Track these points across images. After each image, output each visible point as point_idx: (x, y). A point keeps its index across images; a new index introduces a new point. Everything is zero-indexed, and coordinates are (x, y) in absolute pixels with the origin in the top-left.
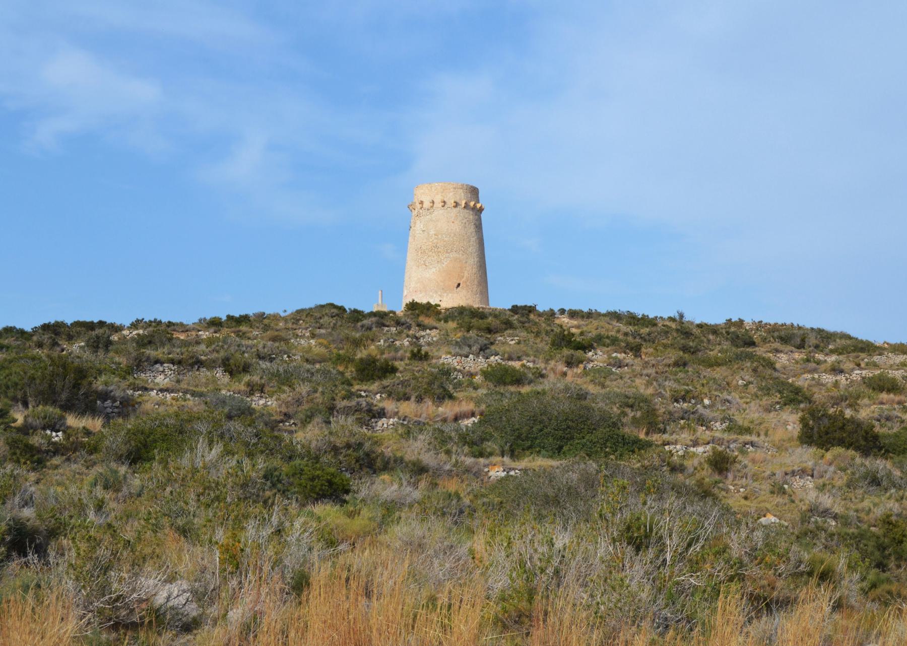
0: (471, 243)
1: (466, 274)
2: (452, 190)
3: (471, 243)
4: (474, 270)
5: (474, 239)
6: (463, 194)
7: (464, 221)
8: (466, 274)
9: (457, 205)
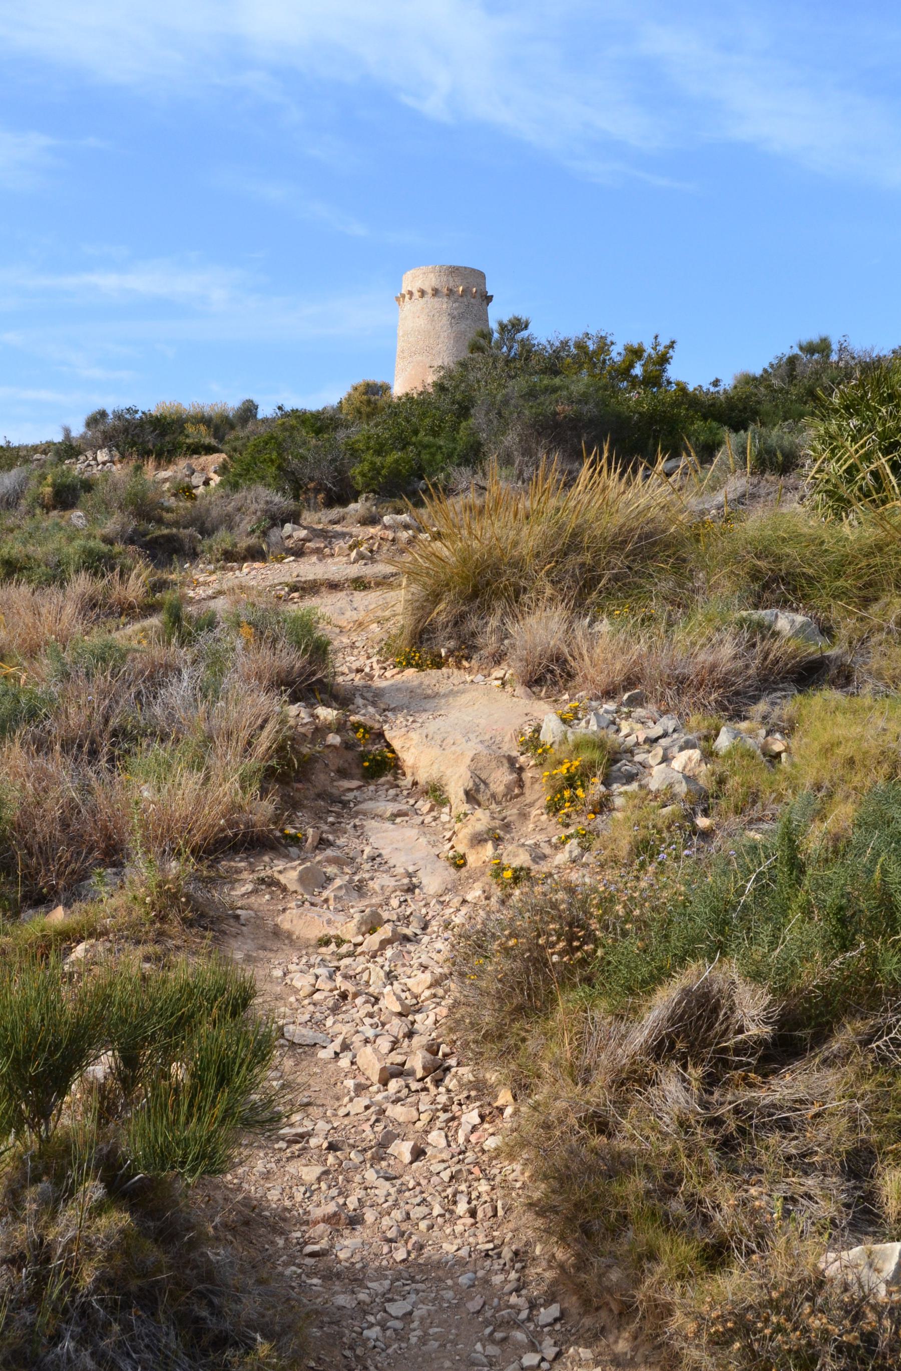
9: (423, 293)
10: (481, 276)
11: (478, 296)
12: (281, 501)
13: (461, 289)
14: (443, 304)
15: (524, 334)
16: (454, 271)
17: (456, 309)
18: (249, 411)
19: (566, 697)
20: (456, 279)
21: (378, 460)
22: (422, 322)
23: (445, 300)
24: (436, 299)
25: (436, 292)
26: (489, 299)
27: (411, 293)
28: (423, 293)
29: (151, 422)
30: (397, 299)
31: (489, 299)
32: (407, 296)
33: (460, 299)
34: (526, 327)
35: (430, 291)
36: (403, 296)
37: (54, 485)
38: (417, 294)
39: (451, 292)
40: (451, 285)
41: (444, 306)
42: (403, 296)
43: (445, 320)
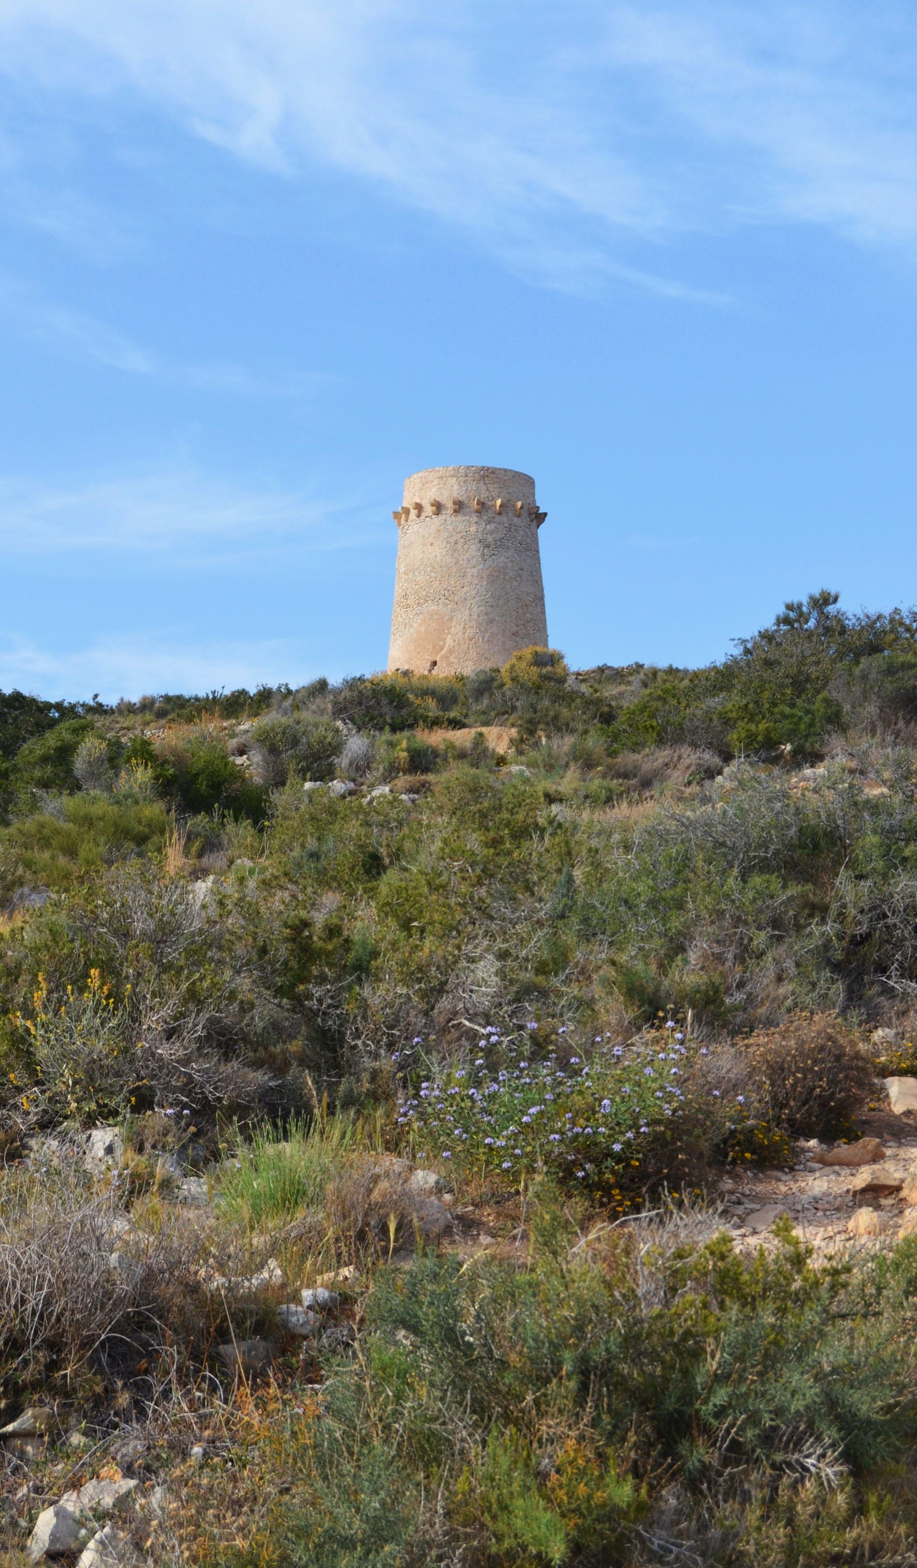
0: (468, 579)
1: (449, 642)
2: (436, 482)
3: (468, 579)
4: (470, 632)
5: (475, 571)
6: (456, 487)
7: (452, 540)
8: (449, 642)
9: (438, 507)
10: (528, 482)
11: (524, 513)
12: (710, 758)
13: (499, 502)
14: (471, 525)
15: (831, 609)
16: (488, 475)
17: (491, 533)
18: (322, 686)
19: (348, 1467)
20: (491, 487)
21: (753, 727)
22: (437, 552)
23: (475, 519)
24: (460, 517)
25: (459, 507)
26: (540, 518)
27: (419, 507)
28: (438, 507)
29: (385, 692)
30: (397, 515)
31: (540, 518)
32: (413, 513)
33: (498, 518)
34: (836, 600)
35: (450, 505)
36: (407, 511)
37: (408, 750)
38: (429, 510)
39: (483, 506)
40: (484, 495)
41: (473, 529)
42: (407, 511)
43: (474, 549)
